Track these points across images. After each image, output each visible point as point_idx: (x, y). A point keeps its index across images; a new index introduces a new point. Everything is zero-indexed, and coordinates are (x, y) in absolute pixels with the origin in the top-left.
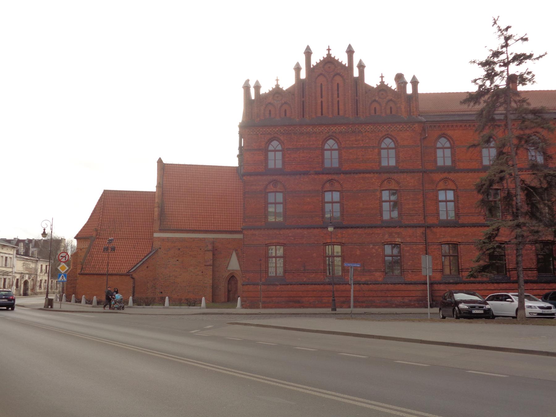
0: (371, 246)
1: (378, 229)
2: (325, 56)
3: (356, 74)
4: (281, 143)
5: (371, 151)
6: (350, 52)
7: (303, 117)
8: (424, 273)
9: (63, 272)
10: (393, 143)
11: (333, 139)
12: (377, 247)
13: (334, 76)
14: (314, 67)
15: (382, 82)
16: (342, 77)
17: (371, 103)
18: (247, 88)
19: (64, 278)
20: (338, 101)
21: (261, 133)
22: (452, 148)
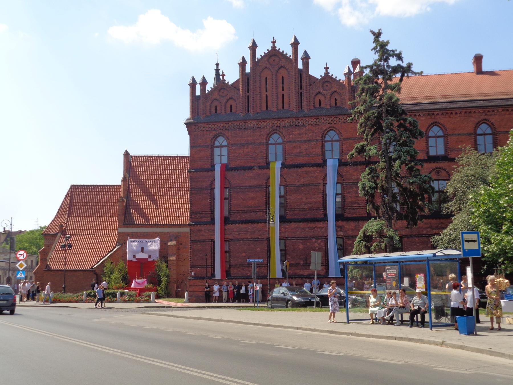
0: (314, 240)
1: (321, 223)
2: (270, 49)
3: (300, 66)
4: (227, 139)
5: (315, 144)
6: (295, 45)
7: (248, 111)
8: (312, 267)
9: (21, 269)
10: (441, 131)
11: (278, 134)
12: (319, 241)
13: (279, 69)
14: (259, 60)
15: (327, 74)
16: (287, 70)
17: (316, 96)
18: (193, 85)
19: (23, 275)
20: (283, 95)
21: (207, 129)
22: (445, 136)
